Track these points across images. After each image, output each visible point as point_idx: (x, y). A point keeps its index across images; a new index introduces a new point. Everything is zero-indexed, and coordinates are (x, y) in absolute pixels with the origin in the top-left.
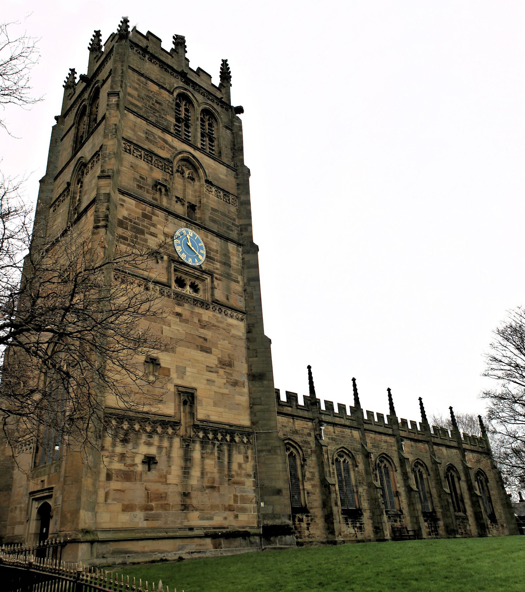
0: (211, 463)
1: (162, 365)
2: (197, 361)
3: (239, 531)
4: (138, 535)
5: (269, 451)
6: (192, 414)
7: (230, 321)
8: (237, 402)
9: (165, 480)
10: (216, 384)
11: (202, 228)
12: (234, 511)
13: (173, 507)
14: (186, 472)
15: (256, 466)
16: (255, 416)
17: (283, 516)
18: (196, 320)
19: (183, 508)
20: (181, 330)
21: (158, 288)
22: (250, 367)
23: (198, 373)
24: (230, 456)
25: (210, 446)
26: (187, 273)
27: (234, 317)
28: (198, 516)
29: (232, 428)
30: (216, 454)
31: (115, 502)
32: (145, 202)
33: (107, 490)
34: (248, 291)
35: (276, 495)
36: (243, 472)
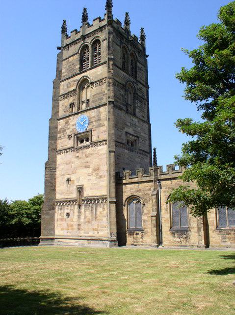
0: (88, 213)
14: (79, 217)
18: (84, 155)
24: (96, 209)
28: (193, 66)
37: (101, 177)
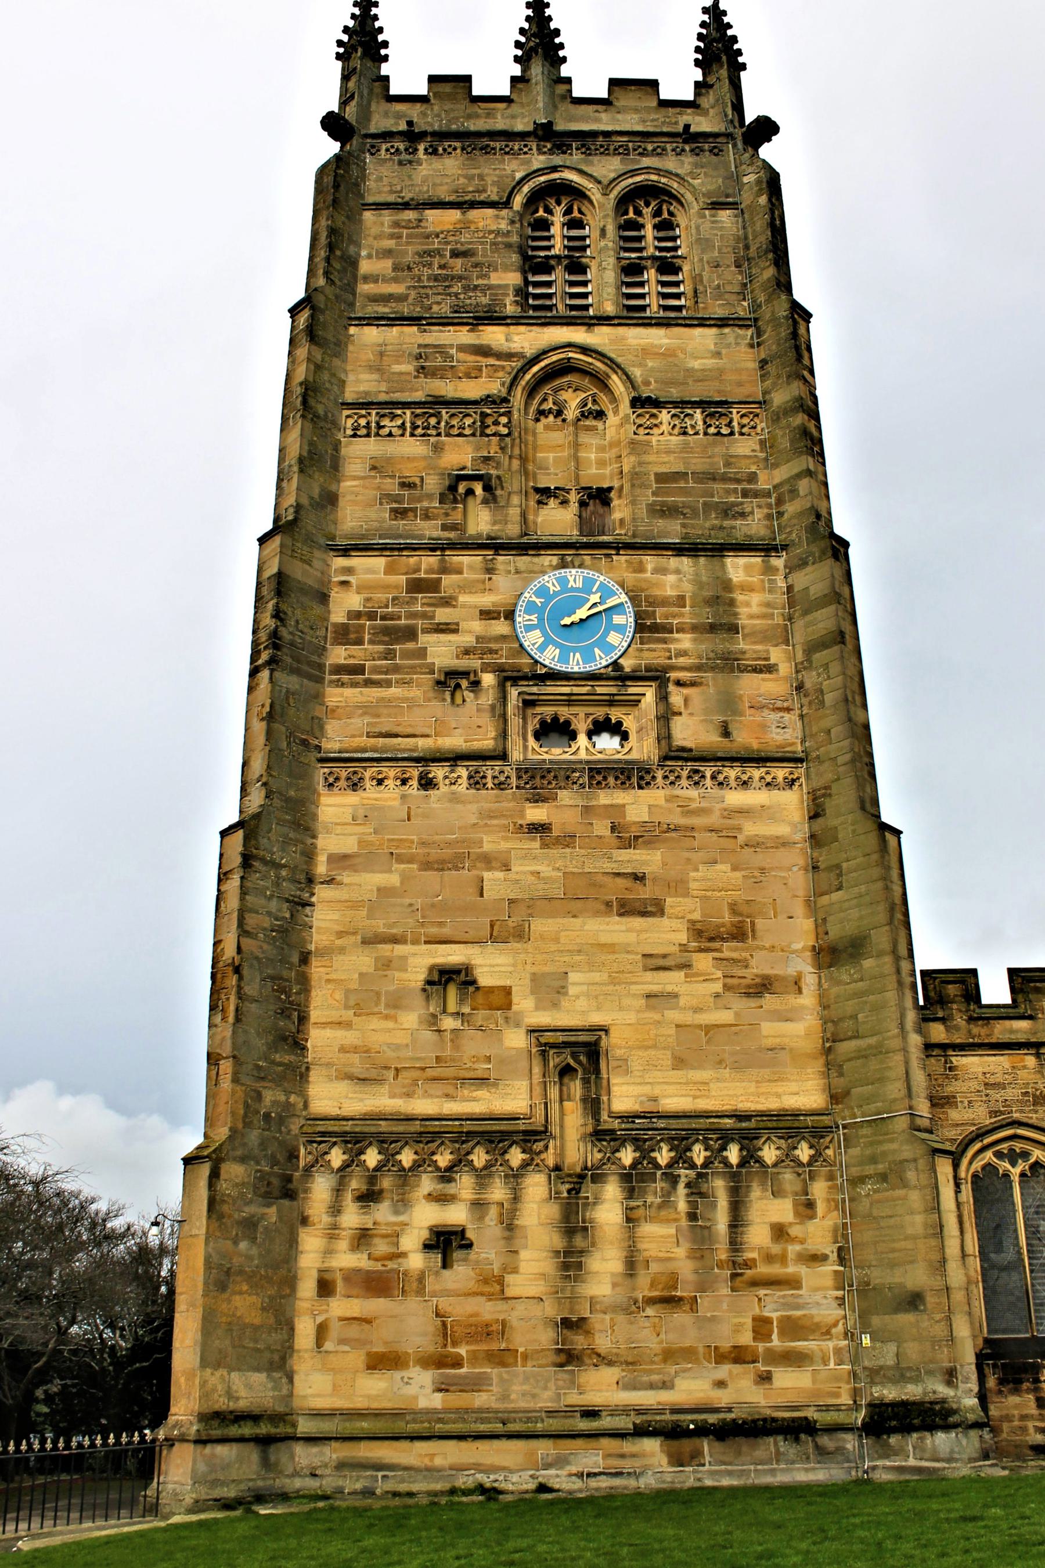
1: (484, 981)
2: (610, 948)
3: (774, 1420)
4: (412, 1427)
5: (884, 1177)
6: (593, 1105)
7: (735, 798)
8: (769, 1042)
9: (498, 1287)
10: (682, 1001)
11: (618, 549)
12: (754, 1362)
13: (525, 1357)
15: (845, 1225)
16: (841, 1075)
17: (930, 1373)
18: (602, 828)
19: (562, 1358)
20: (545, 870)
21: (463, 772)
22: (821, 926)
23: (613, 982)
24: (737, 1208)
25: (660, 1185)
26: (570, 701)
27: (756, 782)
29: (744, 1125)
30: (682, 1206)
31: (347, 1348)
32: (415, 549)
33: (320, 1319)
34: (808, 685)
35: (906, 1311)
36: (793, 1249)
37: (763, 987)
